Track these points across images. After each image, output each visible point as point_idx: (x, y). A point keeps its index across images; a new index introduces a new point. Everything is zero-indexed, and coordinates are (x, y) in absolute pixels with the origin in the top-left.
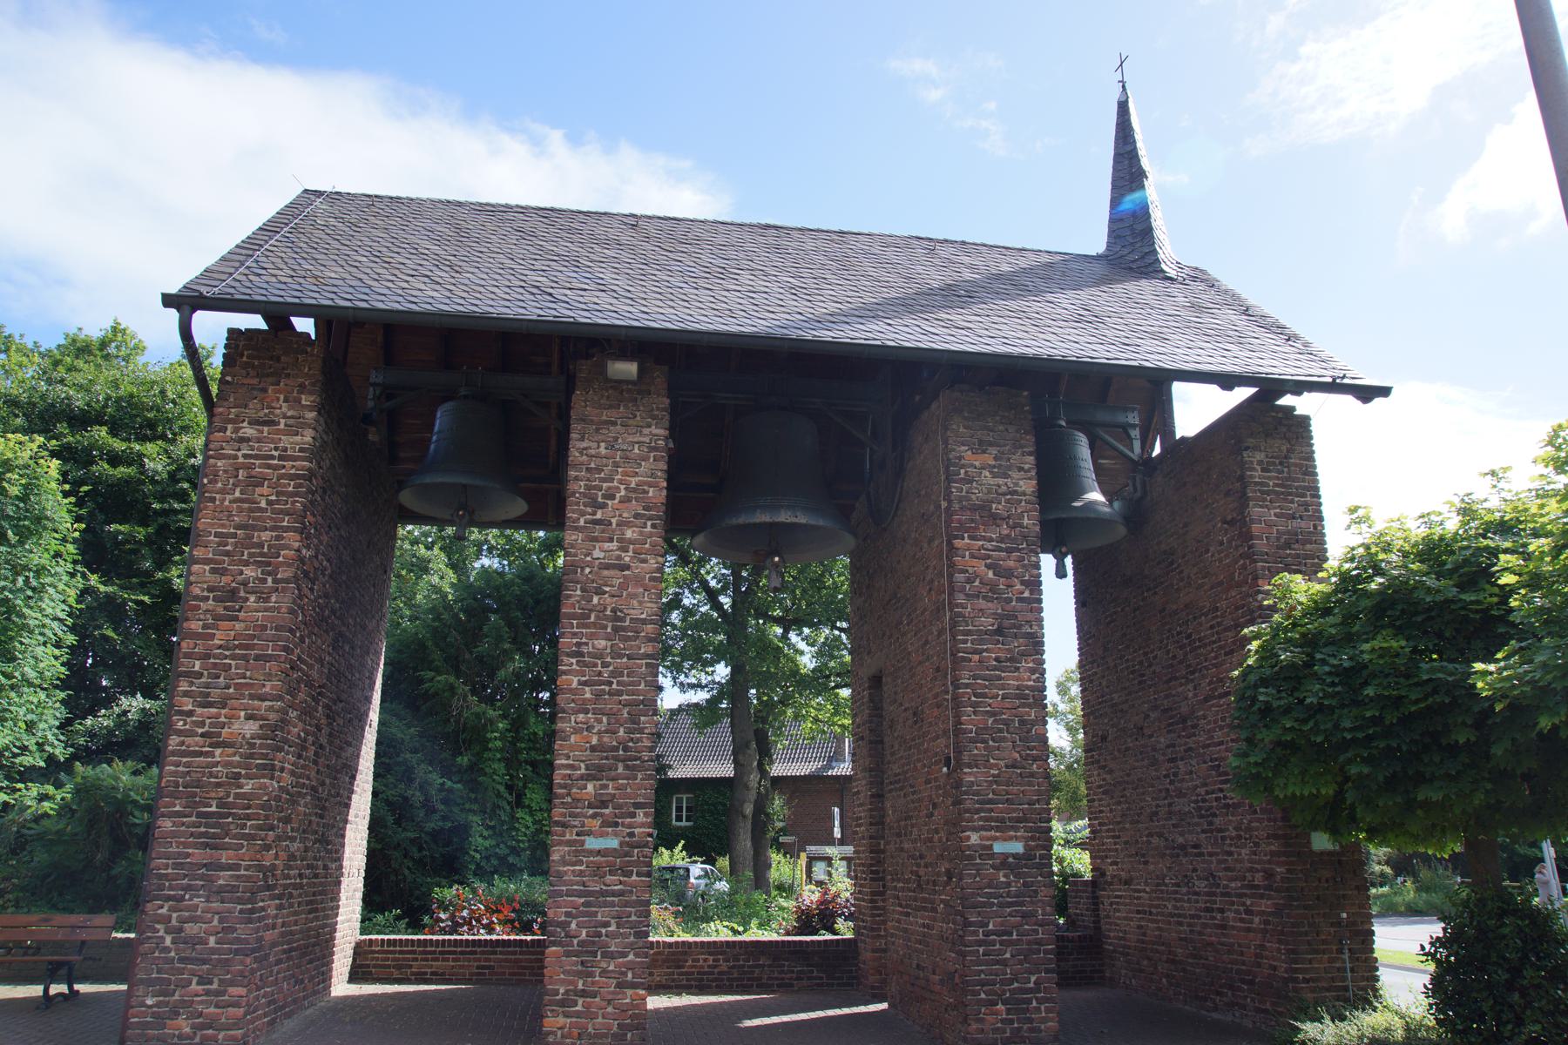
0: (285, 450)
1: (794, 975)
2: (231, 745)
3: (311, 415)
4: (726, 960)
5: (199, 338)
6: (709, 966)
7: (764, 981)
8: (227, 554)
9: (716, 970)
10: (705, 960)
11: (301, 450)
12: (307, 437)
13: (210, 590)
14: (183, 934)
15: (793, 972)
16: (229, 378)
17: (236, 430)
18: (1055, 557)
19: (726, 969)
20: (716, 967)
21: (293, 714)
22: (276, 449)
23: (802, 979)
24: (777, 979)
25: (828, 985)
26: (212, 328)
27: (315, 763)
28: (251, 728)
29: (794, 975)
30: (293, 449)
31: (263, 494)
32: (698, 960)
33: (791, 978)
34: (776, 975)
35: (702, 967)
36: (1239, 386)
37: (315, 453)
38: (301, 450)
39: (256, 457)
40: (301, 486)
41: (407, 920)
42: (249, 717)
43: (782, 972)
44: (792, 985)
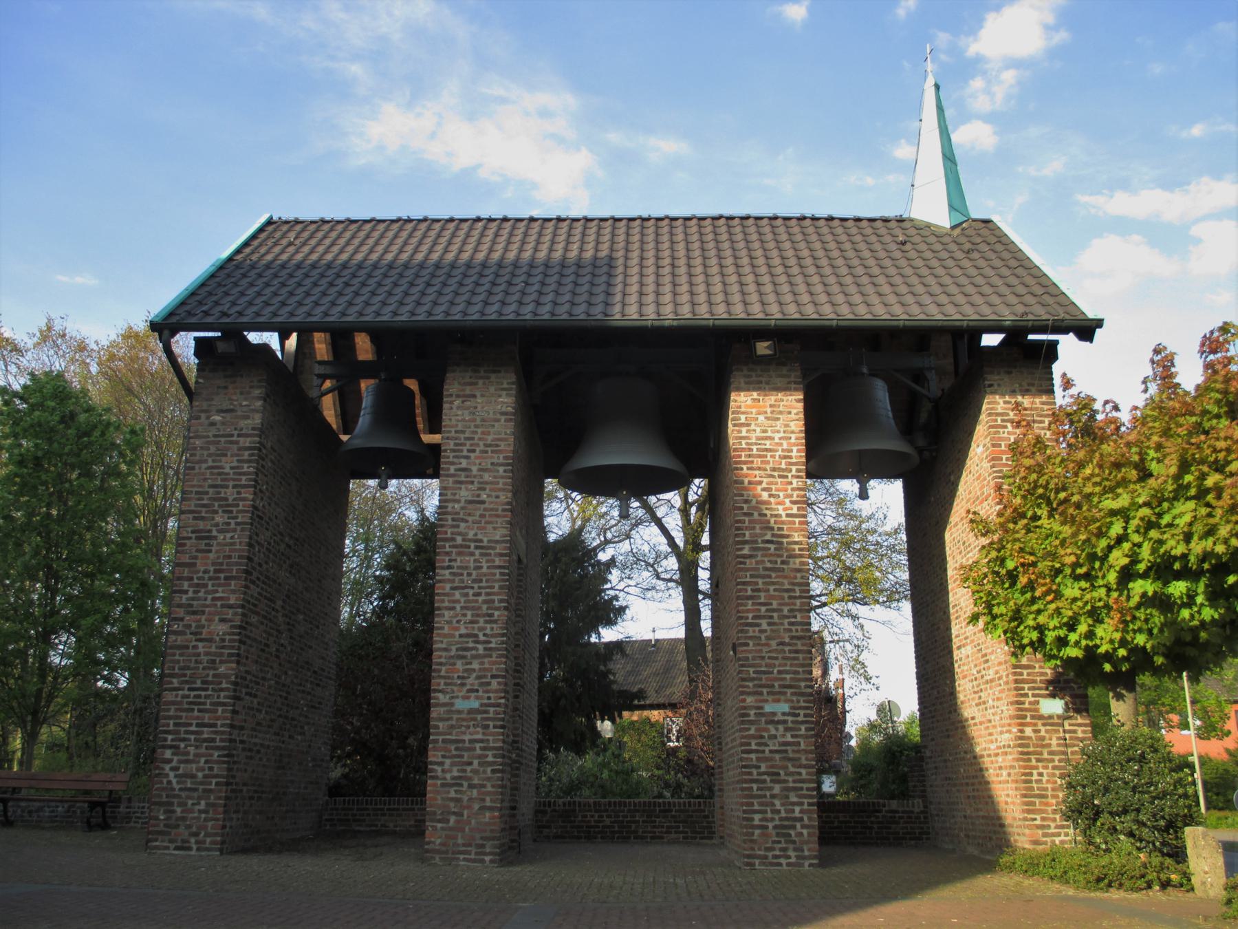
0: (241, 430)
1: (664, 830)
2: (210, 640)
3: (259, 403)
4: (608, 817)
5: (176, 350)
6: (595, 821)
7: (640, 834)
8: (204, 506)
9: (601, 825)
10: (592, 816)
11: (253, 429)
12: (257, 419)
13: (193, 532)
14: (588, 744)
15: (663, 827)
16: (201, 381)
17: (208, 418)
18: (858, 482)
19: (609, 824)
20: (600, 822)
21: (254, 619)
22: (236, 429)
23: (671, 833)
24: (650, 832)
25: (692, 838)
26: (185, 344)
27: (277, 657)
28: (222, 628)
29: (664, 830)
30: (247, 428)
31: (227, 464)
32: (586, 816)
33: (662, 832)
34: (649, 829)
35: (589, 821)
36: (994, 347)
37: (262, 431)
38: (253, 429)
39: (223, 436)
40: (252, 455)
41: (608, 635)
42: (222, 620)
43: (654, 827)
44: (662, 838)
